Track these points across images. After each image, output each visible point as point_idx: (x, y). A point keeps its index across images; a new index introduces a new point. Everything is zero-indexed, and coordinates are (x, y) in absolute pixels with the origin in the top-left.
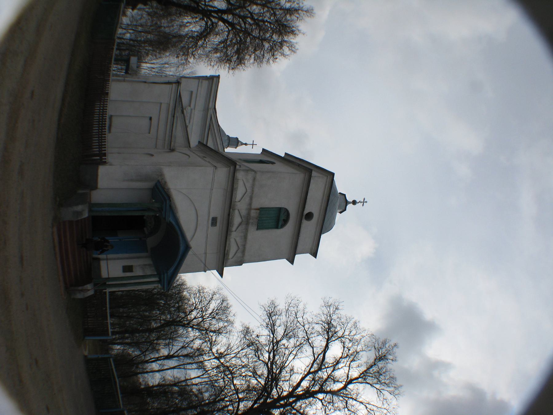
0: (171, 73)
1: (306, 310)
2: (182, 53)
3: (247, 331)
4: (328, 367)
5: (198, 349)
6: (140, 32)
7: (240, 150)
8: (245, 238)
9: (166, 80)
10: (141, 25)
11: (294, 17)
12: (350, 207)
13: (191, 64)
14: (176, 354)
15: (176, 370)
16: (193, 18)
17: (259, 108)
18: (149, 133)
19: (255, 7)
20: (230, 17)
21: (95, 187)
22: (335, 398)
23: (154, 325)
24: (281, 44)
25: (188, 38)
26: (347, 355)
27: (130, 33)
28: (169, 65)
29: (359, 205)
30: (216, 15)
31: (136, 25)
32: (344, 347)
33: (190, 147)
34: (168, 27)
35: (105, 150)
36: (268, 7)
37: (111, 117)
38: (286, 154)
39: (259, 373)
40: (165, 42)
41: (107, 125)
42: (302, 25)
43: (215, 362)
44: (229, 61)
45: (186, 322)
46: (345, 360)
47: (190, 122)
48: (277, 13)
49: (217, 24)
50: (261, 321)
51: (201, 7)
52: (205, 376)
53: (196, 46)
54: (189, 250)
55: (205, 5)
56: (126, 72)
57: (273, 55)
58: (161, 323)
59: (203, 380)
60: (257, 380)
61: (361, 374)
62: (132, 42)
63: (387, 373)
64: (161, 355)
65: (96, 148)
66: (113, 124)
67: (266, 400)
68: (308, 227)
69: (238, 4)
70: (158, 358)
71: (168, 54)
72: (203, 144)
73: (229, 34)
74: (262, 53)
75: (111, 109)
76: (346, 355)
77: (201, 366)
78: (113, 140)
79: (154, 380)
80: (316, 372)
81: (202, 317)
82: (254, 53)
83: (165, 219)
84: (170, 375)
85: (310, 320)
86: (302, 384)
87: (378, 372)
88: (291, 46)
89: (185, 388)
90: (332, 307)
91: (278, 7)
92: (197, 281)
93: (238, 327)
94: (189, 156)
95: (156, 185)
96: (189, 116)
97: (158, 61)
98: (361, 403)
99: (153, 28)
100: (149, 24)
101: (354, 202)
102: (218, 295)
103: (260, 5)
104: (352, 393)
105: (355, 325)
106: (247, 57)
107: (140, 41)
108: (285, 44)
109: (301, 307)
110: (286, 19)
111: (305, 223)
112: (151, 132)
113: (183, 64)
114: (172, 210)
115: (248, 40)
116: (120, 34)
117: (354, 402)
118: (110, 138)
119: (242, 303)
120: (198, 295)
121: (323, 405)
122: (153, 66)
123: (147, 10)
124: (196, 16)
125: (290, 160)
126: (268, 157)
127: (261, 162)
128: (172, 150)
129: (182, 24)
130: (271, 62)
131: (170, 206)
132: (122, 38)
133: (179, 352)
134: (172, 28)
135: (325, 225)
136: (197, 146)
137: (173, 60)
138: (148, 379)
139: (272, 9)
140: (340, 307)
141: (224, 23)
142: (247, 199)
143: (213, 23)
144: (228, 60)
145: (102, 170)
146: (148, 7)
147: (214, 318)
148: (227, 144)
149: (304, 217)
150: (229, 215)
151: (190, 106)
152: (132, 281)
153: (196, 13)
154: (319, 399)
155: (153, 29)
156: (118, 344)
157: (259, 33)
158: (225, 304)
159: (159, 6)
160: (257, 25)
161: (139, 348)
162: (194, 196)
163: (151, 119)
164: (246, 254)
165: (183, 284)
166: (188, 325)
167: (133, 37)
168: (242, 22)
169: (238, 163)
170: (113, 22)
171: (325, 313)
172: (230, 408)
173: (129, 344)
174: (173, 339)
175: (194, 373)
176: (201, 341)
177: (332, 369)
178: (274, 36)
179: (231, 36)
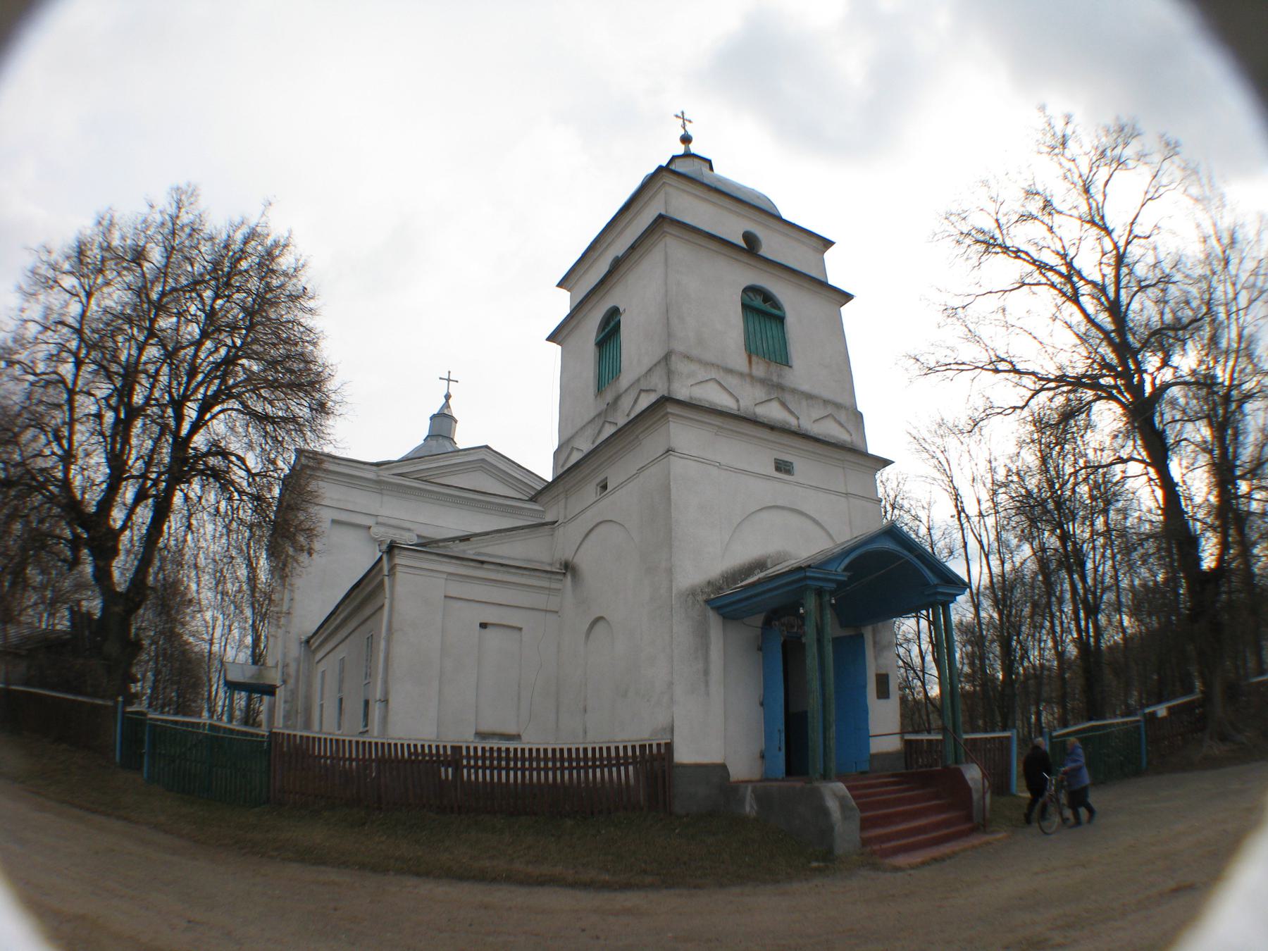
8: (809, 397)
12: (694, 148)
18: (520, 629)
21: (723, 767)
29: (691, 129)
35: (445, 747)
37: (481, 735)
47: (409, 530)
54: (900, 530)
65: (610, 773)
68: (771, 245)
72: (540, 493)
75: (462, 735)
95: (718, 609)
101: (686, 139)
111: (764, 251)
118: (535, 738)
142: (731, 381)
148: (447, 443)
163: (483, 626)
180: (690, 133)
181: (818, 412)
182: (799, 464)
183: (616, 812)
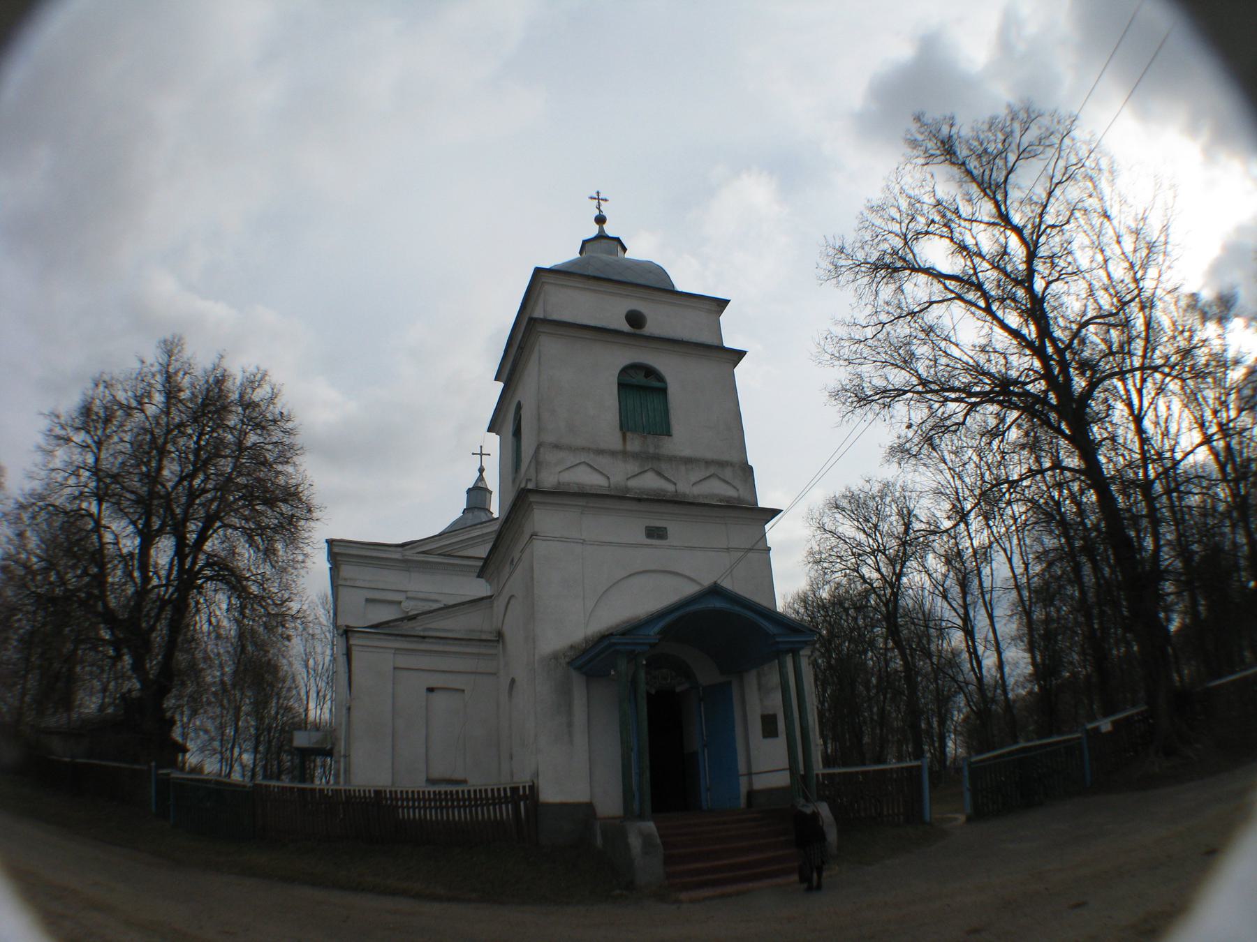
0: (328, 652)
1: (848, 319)
2: (280, 630)
3: (901, 452)
4: (975, 269)
5: (948, 562)
6: (236, 731)
7: (493, 481)
8: (688, 461)
9: (342, 660)
10: (222, 727)
11: (186, 382)
12: (610, 230)
13: (305, 607)
14: (961, 611)
15: (996, 613)
16: (198, 611)
17: (396, 444)
19: (166, 473)
20: (192, 526)
21: (589, 806)
22: (1043, 251)
23: (898, 664)
24: (248, 405)
25: (244, 617)
26: (945, 225)
27: (240, 754)
28: (307, 657)
29: (606, 210)
30: (189, 559)
31: (222, 740)
32: (927, 233)
33: (491, 597)
34: (221, 666)
35: (505, 790)
36: (165, 443)
37: (431, 781)
38: (496, 379)
39: (992, 422)
40: (258, 672)
41: (449, 788)
42: (199, 359)
43: (975, 522)
44: (291, 520)
45: (889, 591)
46: (957, 230)
47: (436, 601)
48: (177, 420)
49: (209, 556)
50: (879, 421)
51: (172, 594)
52: (1007, 545)
53: (263, 598)
54: (722, 588)
55: (167, 586)
56: (329, 753)
57: (275, 421)
58: (893, 649)
59: (1016, 550)
60: (1009, 427)
61: (986, 194)
62: (261, 748)
63: (982, 137)
64: (963, 646)
66: (447, 775)
67: (1052, 407)
68: (660, 320)
69: (161, 511)
70: (970, 654)
71: (285, 661)
73: (229, 526)
74: (270, 447)
75: (415, 782)
76: (945, 229)
77: (983, 554)
78: (481, 776)
79: (1019, 660)
80: (985, 295)
81: (873, 553)
82: (271, 466)
83: (653, 646)
84: (1008, 626)
85: (869, 309)
86: (1014, 326)
87: (979, 156)
88: (252, 382)
89: (1036, 592)
90: (840, 261)
91: (164, 420)
92: (793, 571)
93: (891, 472)
94: (511, 597)
95: (579, 669)
96: (420, 604)
97: (302, 684)
98: (1050, 194)
99: (225, 701)
100: (218, 710)
101: (600, 220)
102: (826, 520)
103: (160, 461)
104: (1030, 215)
105: (878, 209)
106: (281, 480)
107: (257, 729)
108: (247, 397)
109: (841, 331)
110: (191, 400)
111: (651, 328)
112: (462, 687)
113: (305, 625)
114: (632, 629)
115: (242, 480)
116: (243, 776)
117: (1051, 209)
118: (479, 779)
119: (837, 456)
120: (825, 565)
121: (1057, 280)
122: (313, 695)
123: (185, 719)
124: (193, 605)
125: (513, 364)
126: (506, 418)
127: (517, 433)
128: (500, 635)
129: (213, 635)
130: (290, 425)
131: (623, 634)
132: (253, 770)
133: (955, 605)
134: (225, 658)
135: (653, 283)
136: (487, 581)
137: (297, 646)
138: (1019, 675)
139: (169, 432)
140: (838, 244)
141: (206, 539)
142: (602, 462)
143: (208, 565)
144: (290, 523)
145: (549, 795)
146: (177, 717)
147: (876, 526)
149: (638, 331)
150: (639, 500)
151: (400, 603)
152: (796, 715)
153: (188, 605)
154: (1046, 288)
155: (229, 701)
156: (943, 746)
157: (225, 457)
158: (844, 503)
159: (174, 692)
160: (206, 463)
161: (948, 699)
162: (599, 583)
163: (431, 690)
164: (726, 457)
165: (804, 600)
166: (894, 584)
167: (248, 745)
168: (203, 499)
169: (523, 485)
170: (217, 792)
171: (852, 277)
172: (1075, 487)
173: (942, 723)
174: (928, 618)
175: (999, 570)
176: (930, 556)
177: (977, 260)
178: (231, 423)
179: (236, 521)
180: (604, 213)
181: (696, 475)
182: (673, 528)
183: (485, 840)
